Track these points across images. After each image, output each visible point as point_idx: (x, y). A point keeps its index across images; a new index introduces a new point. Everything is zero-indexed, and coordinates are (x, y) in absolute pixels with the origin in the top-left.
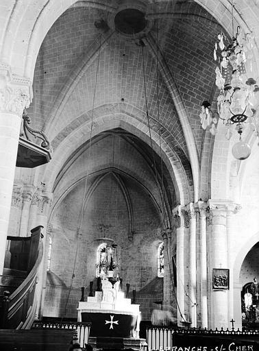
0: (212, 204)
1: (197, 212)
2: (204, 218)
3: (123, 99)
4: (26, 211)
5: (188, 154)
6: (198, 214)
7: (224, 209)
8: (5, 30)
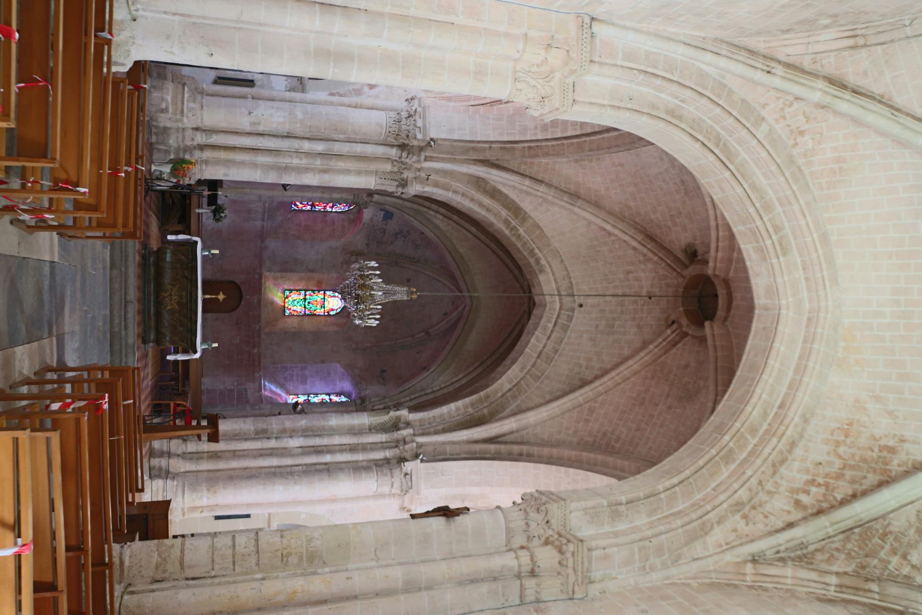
0: (408, 466)
1: (397, 444)
2: (388, 454)
3: (581, 306)
4: (381, 150)
5: (497, 420)
6: (393, 444)
7: (405, 488)
8: (642, 68)
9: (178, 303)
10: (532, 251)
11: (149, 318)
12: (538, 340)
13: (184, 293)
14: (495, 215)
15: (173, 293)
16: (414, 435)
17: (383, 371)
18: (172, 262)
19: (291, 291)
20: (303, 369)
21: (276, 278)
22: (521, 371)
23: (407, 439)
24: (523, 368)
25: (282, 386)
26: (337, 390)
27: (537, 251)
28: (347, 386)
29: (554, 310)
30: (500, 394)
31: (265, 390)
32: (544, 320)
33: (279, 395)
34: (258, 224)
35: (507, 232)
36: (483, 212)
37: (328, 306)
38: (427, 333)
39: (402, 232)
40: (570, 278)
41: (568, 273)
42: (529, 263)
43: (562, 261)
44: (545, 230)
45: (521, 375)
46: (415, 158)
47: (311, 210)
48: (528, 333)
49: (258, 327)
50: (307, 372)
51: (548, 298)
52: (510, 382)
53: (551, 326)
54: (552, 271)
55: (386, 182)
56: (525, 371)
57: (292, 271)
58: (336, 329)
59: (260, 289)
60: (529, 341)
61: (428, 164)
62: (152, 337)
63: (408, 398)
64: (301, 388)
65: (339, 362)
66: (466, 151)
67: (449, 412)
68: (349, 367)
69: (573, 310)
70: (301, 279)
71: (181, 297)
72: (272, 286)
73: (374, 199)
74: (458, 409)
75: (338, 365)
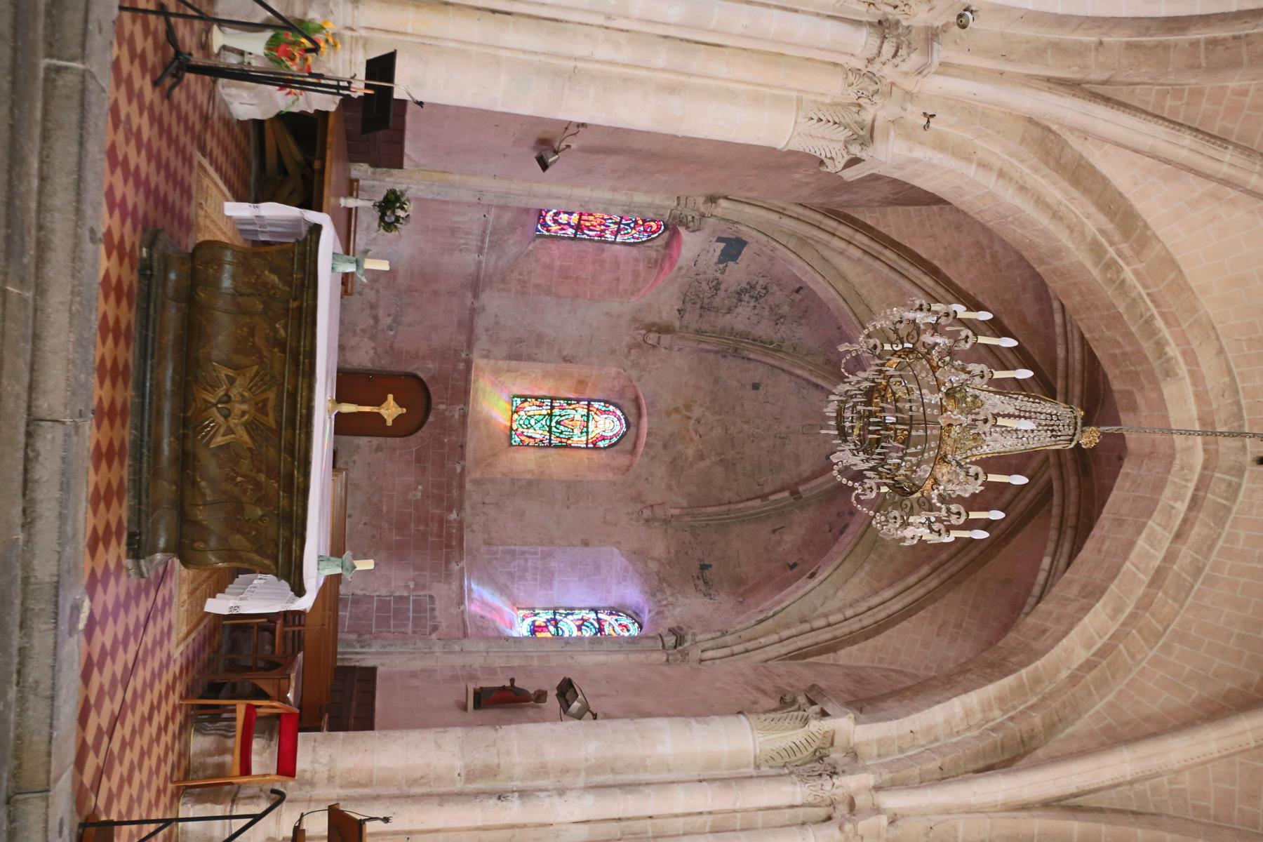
4: (831, 32)
6: (822, 812)
9: (251, 427)
10: (1149, 321)
11: (156, 473)
12: (1151, 542)
13: (272, 395)
14: (1071, 229)
15: (234, 393)
16: (877, 788)
17: (704, 567)
18: (237, 293)
19: (525, 398)
20: (546, 556)
21: (497, 372)
22: (1113, 618)
23: (860, 801)
24: (1117, 610)
25: (503, 590)
26: (612, 601)
27: (1159, 323)
28: (632, 594)
29: (1191, 469)
30: (1064, 674)
31: (471, 600)
32: (1167, 492)
33: (498, 610)
34: (471, 258)
35: (1096, 273)
36: (1044, 221)
37: (594, 431)
38: (794, 493)
39: (753, 287)
40: (1237, 392)
41: (1233, 379)
42: (1139, 351)
43: (1221, 351)
44: (1186, 271)
45: (1114, 627)
46: (915, 59)
47: (574, 238)
48: (1119, 522)
49: (459, 470)
50: (554, 564)
51: (1179, 440)
52: (1088, 645)
53: (1182, 507)
54: (1192, 374)
55: (822, 129)
56: (1122, 618)
57: (531, 358)
58: (611, 476)
59: (466, 392)
60: (1131, 544)
61: (936, 84)
62: (162, 543)
63: (775, 637)
64: (540, 598)
65: (618, 544)
66: (1038, 51)
67: (947, 722)
68: (638, 555)
69: (1240, 471)
70: (546, 375)
71: (261, 408)
72: (489, 388)
73: (718, 212)
74: (968, 713)
75: (616, 551)
